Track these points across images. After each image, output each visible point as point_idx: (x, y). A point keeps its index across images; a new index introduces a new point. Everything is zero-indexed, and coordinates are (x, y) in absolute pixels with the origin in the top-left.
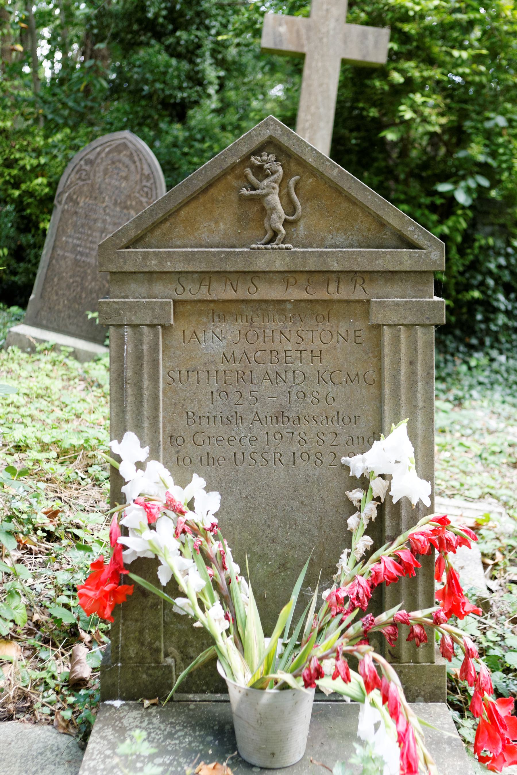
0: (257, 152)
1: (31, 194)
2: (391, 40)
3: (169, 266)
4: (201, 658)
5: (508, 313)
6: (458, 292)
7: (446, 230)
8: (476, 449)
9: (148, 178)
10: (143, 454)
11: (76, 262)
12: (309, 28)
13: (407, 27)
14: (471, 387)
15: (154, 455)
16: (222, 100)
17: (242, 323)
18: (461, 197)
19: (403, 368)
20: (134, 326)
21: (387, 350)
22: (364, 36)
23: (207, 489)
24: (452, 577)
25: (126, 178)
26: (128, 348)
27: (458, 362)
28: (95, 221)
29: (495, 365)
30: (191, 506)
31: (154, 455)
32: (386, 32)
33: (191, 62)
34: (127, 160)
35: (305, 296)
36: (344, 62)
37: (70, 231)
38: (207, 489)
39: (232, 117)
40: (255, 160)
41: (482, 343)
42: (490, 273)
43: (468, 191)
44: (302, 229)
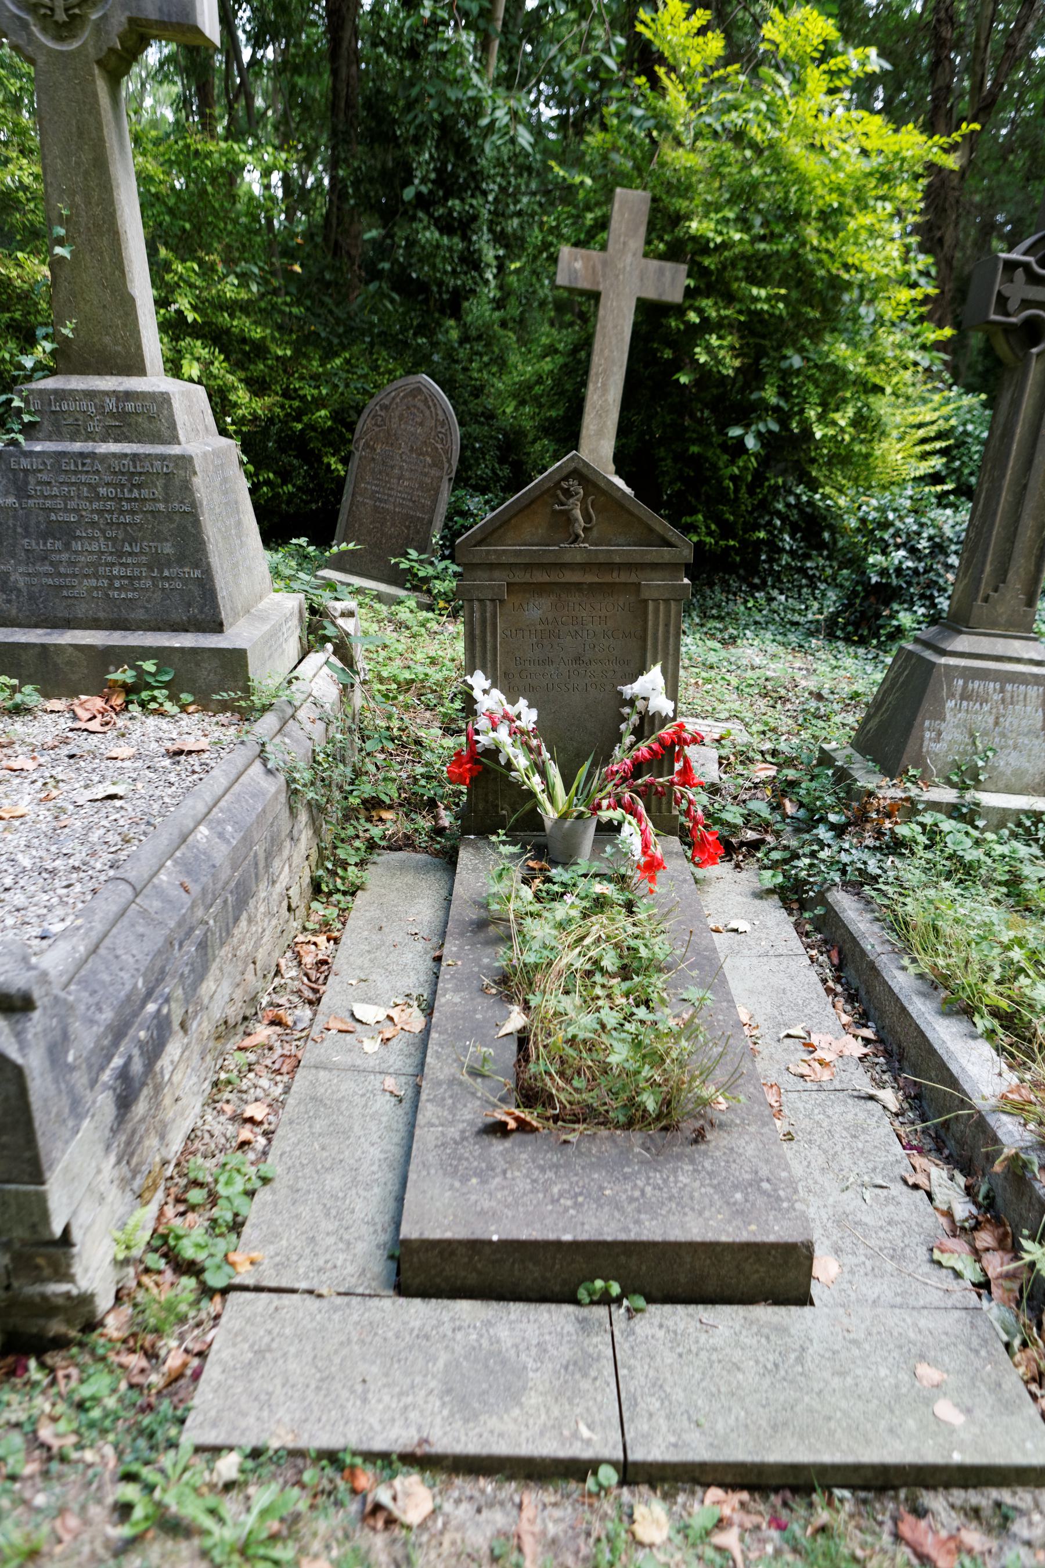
0: (566, 478)
1: (312, 427)
2: (689, 276)
3: (504, 560)
4: (528, 806)
5: (792, 553)
6: (745, 532)
7: (736, 471)
8: (734, 682)
9: (443, 425)
10: (487, 684)
11: (376, 509)
12: (605, 263)
13: (707, 262)
14: (746, 626)
15: (494, 685)
16: (500, 287)
17: (553, 598)
18: (751, 442)
19: (661, 629)
20: (480, 600)
21: (650, 617)
22: (661, 272)
23: (529, 707)
24: (687, 761)
25: (421, 424)
26: (477, 615)
27: (739, 601)
28: (393, 467)
29: (774, 605)
30: (519, 717)
31: (494, 685)
32: (684, 268)
33: (465, 238)
34: (421, 405)
35: (596, 580)
36: (639, 300)
37: (368, 478)
38: (529, 707)
39: (514, 310)
40: (564, 485)
41: (764, 583)
42: (778, 514)
43: (759, 435)
44: (595, 533)
